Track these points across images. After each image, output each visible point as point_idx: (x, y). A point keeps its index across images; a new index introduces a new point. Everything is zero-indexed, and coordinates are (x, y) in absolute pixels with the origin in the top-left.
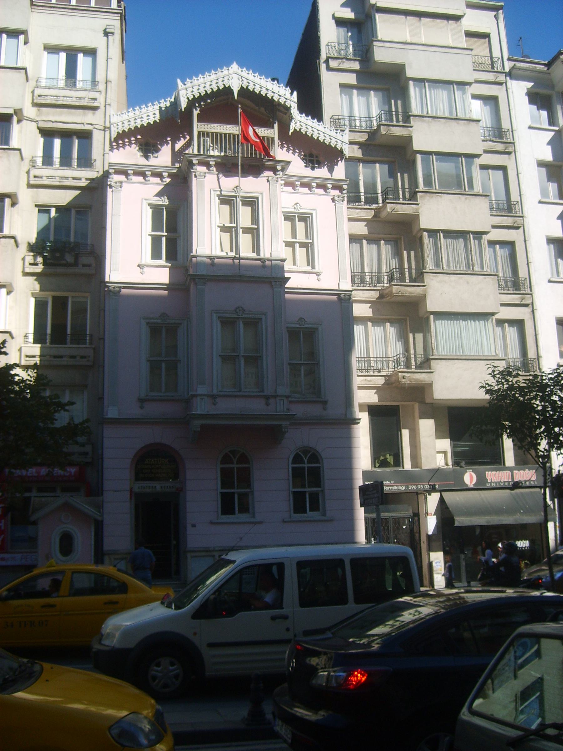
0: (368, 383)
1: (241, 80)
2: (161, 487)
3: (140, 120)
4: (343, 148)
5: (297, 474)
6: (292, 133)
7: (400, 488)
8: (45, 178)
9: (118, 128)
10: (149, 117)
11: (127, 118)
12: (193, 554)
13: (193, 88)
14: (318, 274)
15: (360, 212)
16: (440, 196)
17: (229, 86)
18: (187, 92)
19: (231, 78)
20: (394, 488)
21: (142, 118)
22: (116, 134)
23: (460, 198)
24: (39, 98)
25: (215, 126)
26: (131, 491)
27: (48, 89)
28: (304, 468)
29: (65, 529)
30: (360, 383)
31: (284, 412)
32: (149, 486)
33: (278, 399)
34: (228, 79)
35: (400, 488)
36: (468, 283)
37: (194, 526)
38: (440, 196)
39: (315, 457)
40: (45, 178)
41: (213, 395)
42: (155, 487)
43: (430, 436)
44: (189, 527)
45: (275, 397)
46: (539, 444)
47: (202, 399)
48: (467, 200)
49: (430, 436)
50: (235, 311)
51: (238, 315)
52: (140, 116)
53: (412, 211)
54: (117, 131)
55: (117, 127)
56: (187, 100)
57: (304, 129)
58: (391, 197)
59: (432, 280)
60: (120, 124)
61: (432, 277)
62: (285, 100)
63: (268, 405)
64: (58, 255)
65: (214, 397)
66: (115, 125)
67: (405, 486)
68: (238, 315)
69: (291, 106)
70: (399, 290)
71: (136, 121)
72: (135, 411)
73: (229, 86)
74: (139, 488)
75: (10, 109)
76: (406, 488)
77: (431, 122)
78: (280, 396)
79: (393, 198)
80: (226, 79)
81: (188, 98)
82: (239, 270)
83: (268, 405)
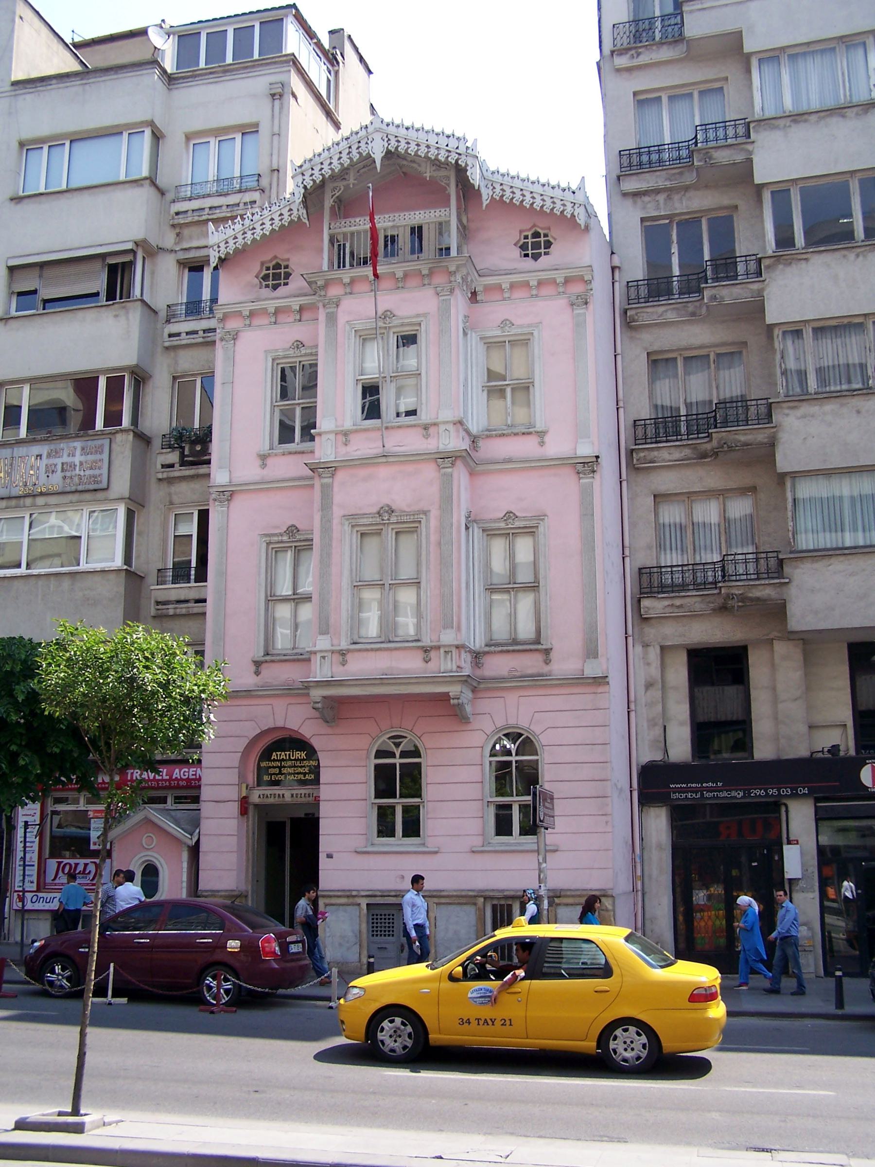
0: (676, 610)
1: (386, 139)
2: (292, 796)
3: (250, 233)
4: (576, 214)
5: (502, 773)
6: (487, 205)
7: (734, 794)
8: (184, 335)
9: (219, 252)
10: (264, 226)
11: (233, 233)
12: (327, 901)
13: (312, 169)
14: (541, 434)
15: (666, 311)
16: (806, 259)
17: (369, 154)
18: (304, 177)
19: (370, 139)
20: (725, 794)
21: (254, 229)
22: (217, 259)
23: (845, 256)
24: (176, 217)
25: (352, 221)
26: (244, 805)
27: (188, 202)
28: (395, 765)
29: (157, 863)
30: (662, 611)
31: (451, 672)
32: (275, 794)
33: (442, 650)
34: (367, 143)
35: (734, 794)
36: (858, 412)
37: (330, 856)
38: (806, 259)
39: (527, 745)
40: (184, 335)
41: (342, 650)
42: (283, 795)
43: (796, 699)
44: (322, 857)
45: (438, 648)
46: (56, 752)
47: (324, 657)
48: (861, 258)
49: (796, 699)
50: (378, 513)
51: (383, 520)
52: (251, 227)
53: (750, 295)
54: (217, 255)
55: (217, 250)
56: (303, 191)
57: (507, 196)
58: (722, 275)
59: (787, 415)
60: (222, 245)
61: (787, 411)
62: (457, 156)
63: (427, 662)
64: (198, 448)
65: (343, 653)
66: (215, 248)
67: (744, 790)
68: (383, 520)
69: (467, 165)
70: (723, 442)
71: (246, 235)
72: (247, 680)
73: (369, 154)
74: (259, 797)
75: (128, 243)
76: (744, 793)
77: (790, 126)
78: (445, 646)
79: (727, 277)
80: (363, 144)
81: (305, 187)
82: (384, 446)
83: (427, 662)
